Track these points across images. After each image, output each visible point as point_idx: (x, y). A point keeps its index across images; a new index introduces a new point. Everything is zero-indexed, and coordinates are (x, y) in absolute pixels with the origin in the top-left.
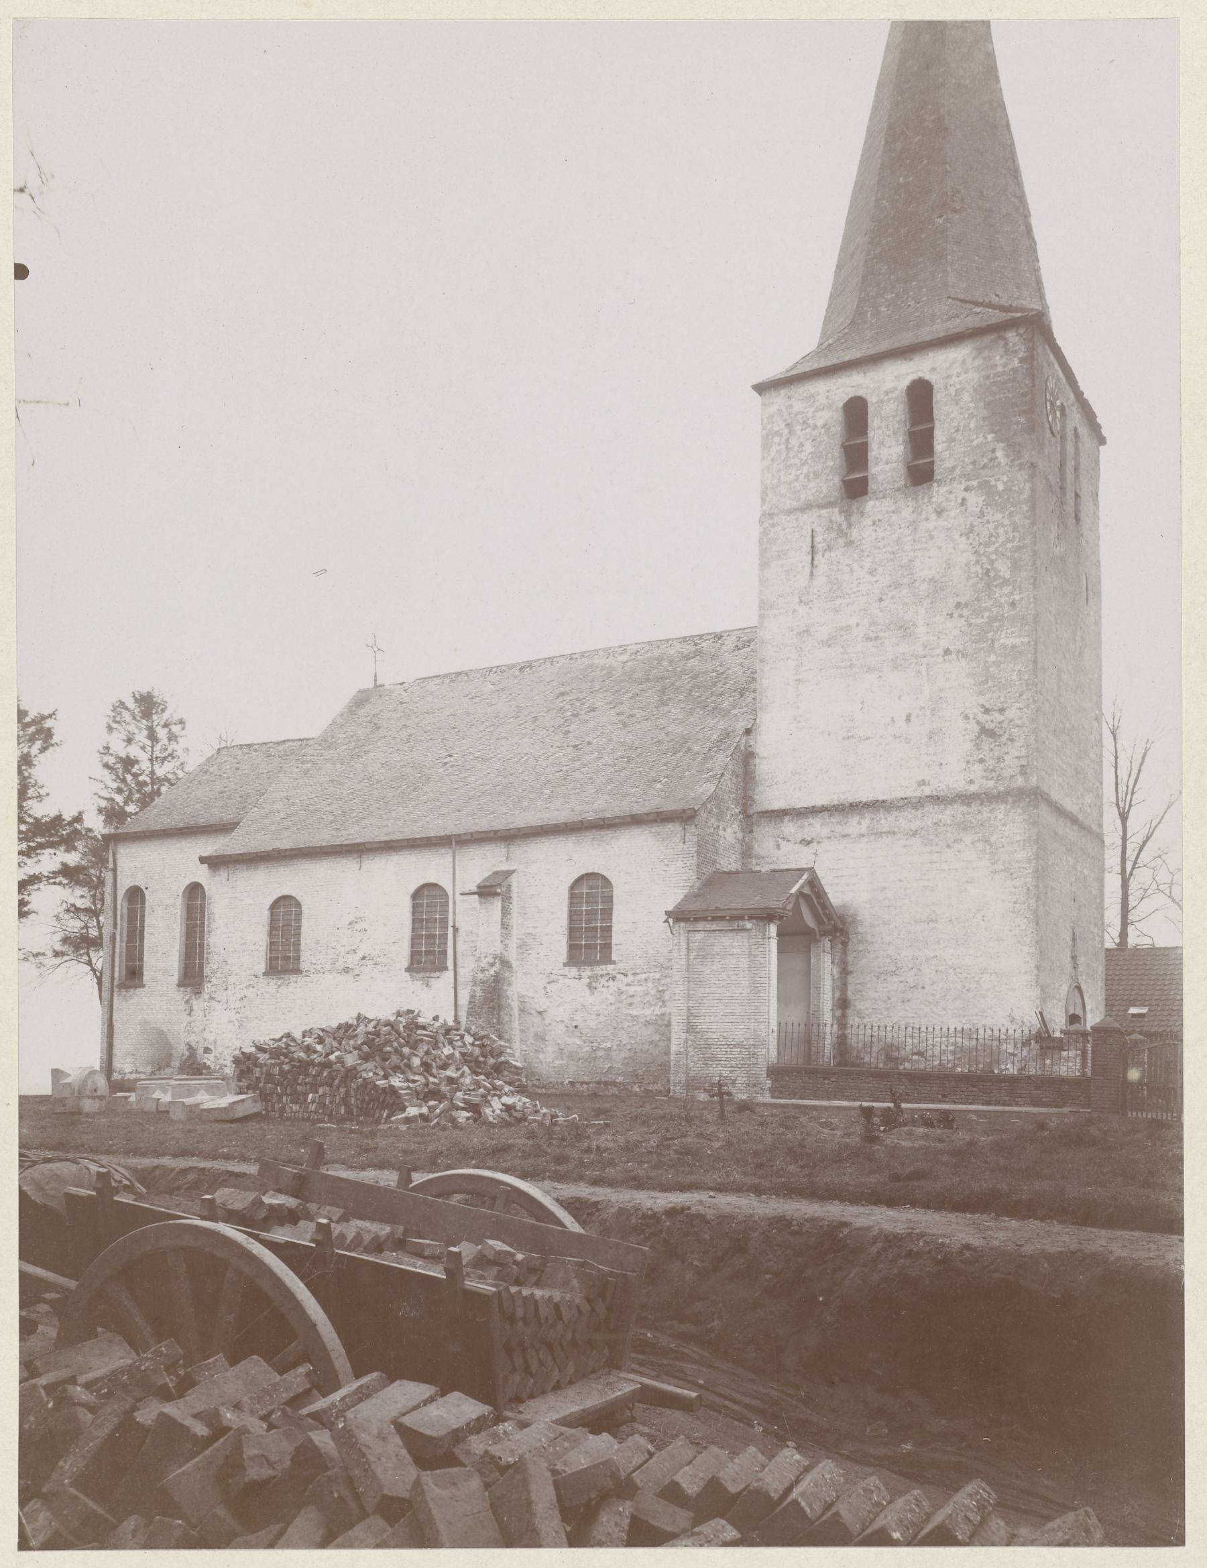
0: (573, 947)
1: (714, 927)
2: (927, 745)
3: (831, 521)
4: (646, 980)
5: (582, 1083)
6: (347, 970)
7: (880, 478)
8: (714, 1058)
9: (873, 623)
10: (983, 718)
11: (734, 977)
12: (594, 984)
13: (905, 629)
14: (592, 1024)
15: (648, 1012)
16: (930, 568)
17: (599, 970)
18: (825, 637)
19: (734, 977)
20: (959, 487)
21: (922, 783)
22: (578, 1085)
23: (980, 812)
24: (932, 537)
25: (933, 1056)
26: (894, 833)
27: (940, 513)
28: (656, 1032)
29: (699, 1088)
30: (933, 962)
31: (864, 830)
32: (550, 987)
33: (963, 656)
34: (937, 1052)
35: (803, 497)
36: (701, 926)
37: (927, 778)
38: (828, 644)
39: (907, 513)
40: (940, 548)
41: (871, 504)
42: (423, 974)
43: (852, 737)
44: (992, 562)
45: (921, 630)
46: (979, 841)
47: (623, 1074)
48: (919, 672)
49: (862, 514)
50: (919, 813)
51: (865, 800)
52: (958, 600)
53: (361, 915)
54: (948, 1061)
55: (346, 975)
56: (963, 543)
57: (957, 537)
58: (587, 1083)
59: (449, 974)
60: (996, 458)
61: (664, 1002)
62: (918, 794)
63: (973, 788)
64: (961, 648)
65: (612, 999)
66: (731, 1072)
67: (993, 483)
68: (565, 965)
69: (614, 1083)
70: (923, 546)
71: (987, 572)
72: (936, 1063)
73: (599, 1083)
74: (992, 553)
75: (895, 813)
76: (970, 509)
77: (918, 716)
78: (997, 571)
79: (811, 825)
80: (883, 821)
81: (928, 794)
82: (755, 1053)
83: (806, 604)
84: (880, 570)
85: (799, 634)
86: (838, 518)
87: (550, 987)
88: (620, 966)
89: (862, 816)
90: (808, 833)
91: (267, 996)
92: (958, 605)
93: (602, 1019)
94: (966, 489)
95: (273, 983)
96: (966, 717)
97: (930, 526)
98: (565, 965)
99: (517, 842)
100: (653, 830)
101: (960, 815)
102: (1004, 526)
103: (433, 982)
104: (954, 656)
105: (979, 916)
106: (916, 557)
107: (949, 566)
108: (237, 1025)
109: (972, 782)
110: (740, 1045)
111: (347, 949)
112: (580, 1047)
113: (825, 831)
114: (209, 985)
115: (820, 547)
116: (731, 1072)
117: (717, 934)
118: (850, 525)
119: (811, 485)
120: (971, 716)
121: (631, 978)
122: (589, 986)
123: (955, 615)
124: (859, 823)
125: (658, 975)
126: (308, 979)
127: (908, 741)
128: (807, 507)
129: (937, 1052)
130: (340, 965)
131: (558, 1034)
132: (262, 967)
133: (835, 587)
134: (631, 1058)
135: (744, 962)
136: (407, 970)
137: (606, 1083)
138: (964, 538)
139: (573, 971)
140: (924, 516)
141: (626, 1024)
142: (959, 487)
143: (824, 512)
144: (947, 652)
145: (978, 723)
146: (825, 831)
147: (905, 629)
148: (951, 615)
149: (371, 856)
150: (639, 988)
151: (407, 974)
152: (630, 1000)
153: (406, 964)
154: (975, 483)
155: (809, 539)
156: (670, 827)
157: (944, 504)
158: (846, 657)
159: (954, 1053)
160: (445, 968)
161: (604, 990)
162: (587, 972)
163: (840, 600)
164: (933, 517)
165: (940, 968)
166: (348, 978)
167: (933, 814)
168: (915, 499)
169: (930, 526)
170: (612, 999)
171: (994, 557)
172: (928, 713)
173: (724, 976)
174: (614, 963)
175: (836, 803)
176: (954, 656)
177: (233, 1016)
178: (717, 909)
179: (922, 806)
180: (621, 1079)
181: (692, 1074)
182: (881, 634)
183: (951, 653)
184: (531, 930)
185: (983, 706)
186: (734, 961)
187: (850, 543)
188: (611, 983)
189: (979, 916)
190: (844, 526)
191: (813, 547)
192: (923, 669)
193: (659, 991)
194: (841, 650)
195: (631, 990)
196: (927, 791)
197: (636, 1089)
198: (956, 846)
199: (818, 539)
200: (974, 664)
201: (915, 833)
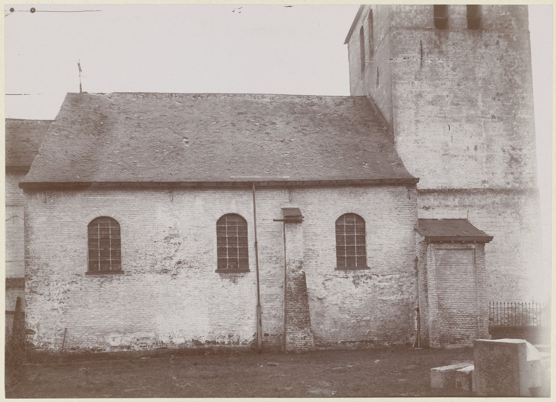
0: (340, 258)
1: (452, 247)
2: (486, 163)
3: (431, 39)
4: (390, 279)
5: (350, 342)
6: (165, 271)
7: (455, 21)
8: (455, 324)
9: (456, 96)
10: (512, 152)
11: (464, 276)
12: (357, 281)
13: (472, 103)
14: (357, 306)
15: (393, 298)
16: (483, 73)
17: (359, 273)
18: (430, 100)
19: (464, 276)
20: (495, 36)
21: (484, 182)
22: (348, 344)
23: (514, 199)
24: (483, 58)
25: (498, 320)
26: (472, 206)
27: (487, 46)
28: (399, 309)
29: (446, 342)
30: (495, 272)
31: (457, 204)
32: (327, 283)
33: (501, 120)
34: (499, 318)
35: (414, 22)
36: (444, 246)
37: (487, 179)
38: (432, 103)
39: (470, 42)
40: (487, 64)
41: (451, 34)
42: (229, 274)
43: (447, 154)
44: (513, 76)
45: (480, 103)
46: (514, 213)
47: (378, 335)
48: (480, 125)
49: (447, 38)
50: (484, 197)
51: (456, 188)
52: (498, 91)
53: (176, 232)
54: (505, 323)
55: (165, 275)
56: (498, 64)
57: (495, 60)
58: (353, 342)
59: (252, 275)
60: (512, 24)
61: (402, 292)
62: (483, 187)
63: (509, 186)
64: (500, 116)
65: (370, 290)
66: (466, 331)
67: (511, 36)
68: (336, 269)
69: (371, 341)
70: (479, 61)
71: (511, 80)
72: (499, 324)
73: (362, 341)
74: (512, 71)
75: (472, 196)
76: (502, 47)
77: (480, 147)
78: (515, 81)
79: (428, 199)
80: (466, 200)
81: (488, 187)
82: (481, 320)
83: (419, 80)
84: (458, 69)
85: (416, 96)
86: (434, 37)
87: (327, 283)
88: (373, 270)
89: (455, 197)
90: (427, 203)
91: (90, 290)
92: (498, 94)
93: (363, 302)
94: (499, 37)
95: (96, 280)
96: (504, 151)
97: (482, 51)
98: (336, 269)
99: (297, 191)
100: (390, 190)
101: (504, 199)
102: (517, 59)
103: (239, 280)
104: (496, 119)
105: (516, 250)
106: (475, 66)
107: (492, 73)
108: (61, 312)
109: (508, 183)
110: (470, 315)
111: (164, 256)
112: (348, 320)
113: (436, 203)
114: (30, 282)
115: (426, 51)
116: (466, 331)
117: (453, 251)
118: (441, 43)
119: (419, 16)
120: (506, 151)
121: (381, 278)
122: (354, 282)
123: (496, 99)
124: (454, 200)
125: (398, 276)
126: (129, 277)
127: (476, 160)
128: (417, 28)
129: (499, 319)
130: (158, 267)
131: (333, 312)
132: (85, 268)
133: (435, 74)
134: (383, 326)
135: (470, 268)
136: (216, 271)
137: (366, 342)
138: (499, 61)
139: (342, 273)
140: (479, 45)
141: (379, 306)
142: (495, 36)
143: (426, 32)
144: (493, 117)
145: (510, 154)
146: (436, 203)
147: (472, 103)
148: (494, 99)
149: (182, 192)
150: (387, 284)
151: (217, 274)
152: (381, 291)
153: (216, 268)
154: (503, 34)
155: (419, 46)
156: (400, 189)
157: (488, 42)
158: (442, 111)
159: (508, 318)
160: (248, 271)
161: (365, 285)
162: (351, 274)
163: (437, 82)
164: (483, 47)
165: (498, 276)
166: (168, 277)
167: (490, 199)
168: (474, 36)
169: (482, 51)
170: (370, 290)
171: (513, 73)
172: (485, 146)
173: (458, 276)
174: (369, 268)
175: (440, 188)
176: (496, 119)
177: (56, 305)
178: (458, 236)
179: (486, 193)
180: (376, 338)
181: (442, 333)
182: (460, 103)
183: (495, 118)
184: (311, 247)
185: (511, 146)
186: (464, 267)
187: (441, 52)
188: (369, 280)
189: (516, 250)
190: (438, 43)
191: (421, 50)
192: (482, 123)
193: (399, 286)
194: (439, 108)
195: (382, 285)
196: (487, 186)
197: (386, 344)
198: (503, 214)
199: (425, 46)
200: (506, 125)
201: (483, 207)
